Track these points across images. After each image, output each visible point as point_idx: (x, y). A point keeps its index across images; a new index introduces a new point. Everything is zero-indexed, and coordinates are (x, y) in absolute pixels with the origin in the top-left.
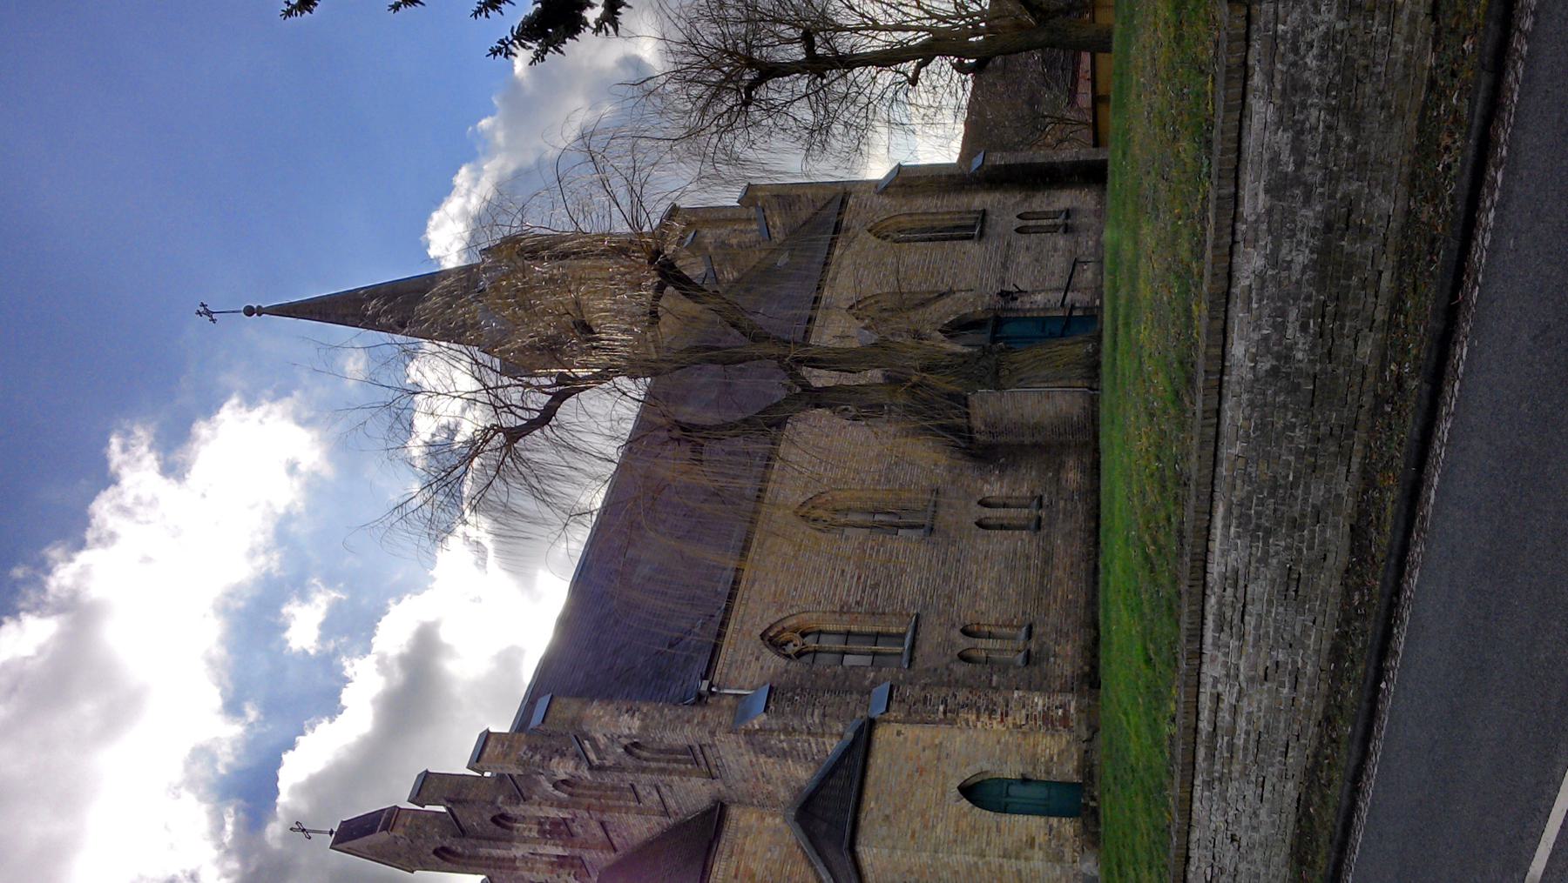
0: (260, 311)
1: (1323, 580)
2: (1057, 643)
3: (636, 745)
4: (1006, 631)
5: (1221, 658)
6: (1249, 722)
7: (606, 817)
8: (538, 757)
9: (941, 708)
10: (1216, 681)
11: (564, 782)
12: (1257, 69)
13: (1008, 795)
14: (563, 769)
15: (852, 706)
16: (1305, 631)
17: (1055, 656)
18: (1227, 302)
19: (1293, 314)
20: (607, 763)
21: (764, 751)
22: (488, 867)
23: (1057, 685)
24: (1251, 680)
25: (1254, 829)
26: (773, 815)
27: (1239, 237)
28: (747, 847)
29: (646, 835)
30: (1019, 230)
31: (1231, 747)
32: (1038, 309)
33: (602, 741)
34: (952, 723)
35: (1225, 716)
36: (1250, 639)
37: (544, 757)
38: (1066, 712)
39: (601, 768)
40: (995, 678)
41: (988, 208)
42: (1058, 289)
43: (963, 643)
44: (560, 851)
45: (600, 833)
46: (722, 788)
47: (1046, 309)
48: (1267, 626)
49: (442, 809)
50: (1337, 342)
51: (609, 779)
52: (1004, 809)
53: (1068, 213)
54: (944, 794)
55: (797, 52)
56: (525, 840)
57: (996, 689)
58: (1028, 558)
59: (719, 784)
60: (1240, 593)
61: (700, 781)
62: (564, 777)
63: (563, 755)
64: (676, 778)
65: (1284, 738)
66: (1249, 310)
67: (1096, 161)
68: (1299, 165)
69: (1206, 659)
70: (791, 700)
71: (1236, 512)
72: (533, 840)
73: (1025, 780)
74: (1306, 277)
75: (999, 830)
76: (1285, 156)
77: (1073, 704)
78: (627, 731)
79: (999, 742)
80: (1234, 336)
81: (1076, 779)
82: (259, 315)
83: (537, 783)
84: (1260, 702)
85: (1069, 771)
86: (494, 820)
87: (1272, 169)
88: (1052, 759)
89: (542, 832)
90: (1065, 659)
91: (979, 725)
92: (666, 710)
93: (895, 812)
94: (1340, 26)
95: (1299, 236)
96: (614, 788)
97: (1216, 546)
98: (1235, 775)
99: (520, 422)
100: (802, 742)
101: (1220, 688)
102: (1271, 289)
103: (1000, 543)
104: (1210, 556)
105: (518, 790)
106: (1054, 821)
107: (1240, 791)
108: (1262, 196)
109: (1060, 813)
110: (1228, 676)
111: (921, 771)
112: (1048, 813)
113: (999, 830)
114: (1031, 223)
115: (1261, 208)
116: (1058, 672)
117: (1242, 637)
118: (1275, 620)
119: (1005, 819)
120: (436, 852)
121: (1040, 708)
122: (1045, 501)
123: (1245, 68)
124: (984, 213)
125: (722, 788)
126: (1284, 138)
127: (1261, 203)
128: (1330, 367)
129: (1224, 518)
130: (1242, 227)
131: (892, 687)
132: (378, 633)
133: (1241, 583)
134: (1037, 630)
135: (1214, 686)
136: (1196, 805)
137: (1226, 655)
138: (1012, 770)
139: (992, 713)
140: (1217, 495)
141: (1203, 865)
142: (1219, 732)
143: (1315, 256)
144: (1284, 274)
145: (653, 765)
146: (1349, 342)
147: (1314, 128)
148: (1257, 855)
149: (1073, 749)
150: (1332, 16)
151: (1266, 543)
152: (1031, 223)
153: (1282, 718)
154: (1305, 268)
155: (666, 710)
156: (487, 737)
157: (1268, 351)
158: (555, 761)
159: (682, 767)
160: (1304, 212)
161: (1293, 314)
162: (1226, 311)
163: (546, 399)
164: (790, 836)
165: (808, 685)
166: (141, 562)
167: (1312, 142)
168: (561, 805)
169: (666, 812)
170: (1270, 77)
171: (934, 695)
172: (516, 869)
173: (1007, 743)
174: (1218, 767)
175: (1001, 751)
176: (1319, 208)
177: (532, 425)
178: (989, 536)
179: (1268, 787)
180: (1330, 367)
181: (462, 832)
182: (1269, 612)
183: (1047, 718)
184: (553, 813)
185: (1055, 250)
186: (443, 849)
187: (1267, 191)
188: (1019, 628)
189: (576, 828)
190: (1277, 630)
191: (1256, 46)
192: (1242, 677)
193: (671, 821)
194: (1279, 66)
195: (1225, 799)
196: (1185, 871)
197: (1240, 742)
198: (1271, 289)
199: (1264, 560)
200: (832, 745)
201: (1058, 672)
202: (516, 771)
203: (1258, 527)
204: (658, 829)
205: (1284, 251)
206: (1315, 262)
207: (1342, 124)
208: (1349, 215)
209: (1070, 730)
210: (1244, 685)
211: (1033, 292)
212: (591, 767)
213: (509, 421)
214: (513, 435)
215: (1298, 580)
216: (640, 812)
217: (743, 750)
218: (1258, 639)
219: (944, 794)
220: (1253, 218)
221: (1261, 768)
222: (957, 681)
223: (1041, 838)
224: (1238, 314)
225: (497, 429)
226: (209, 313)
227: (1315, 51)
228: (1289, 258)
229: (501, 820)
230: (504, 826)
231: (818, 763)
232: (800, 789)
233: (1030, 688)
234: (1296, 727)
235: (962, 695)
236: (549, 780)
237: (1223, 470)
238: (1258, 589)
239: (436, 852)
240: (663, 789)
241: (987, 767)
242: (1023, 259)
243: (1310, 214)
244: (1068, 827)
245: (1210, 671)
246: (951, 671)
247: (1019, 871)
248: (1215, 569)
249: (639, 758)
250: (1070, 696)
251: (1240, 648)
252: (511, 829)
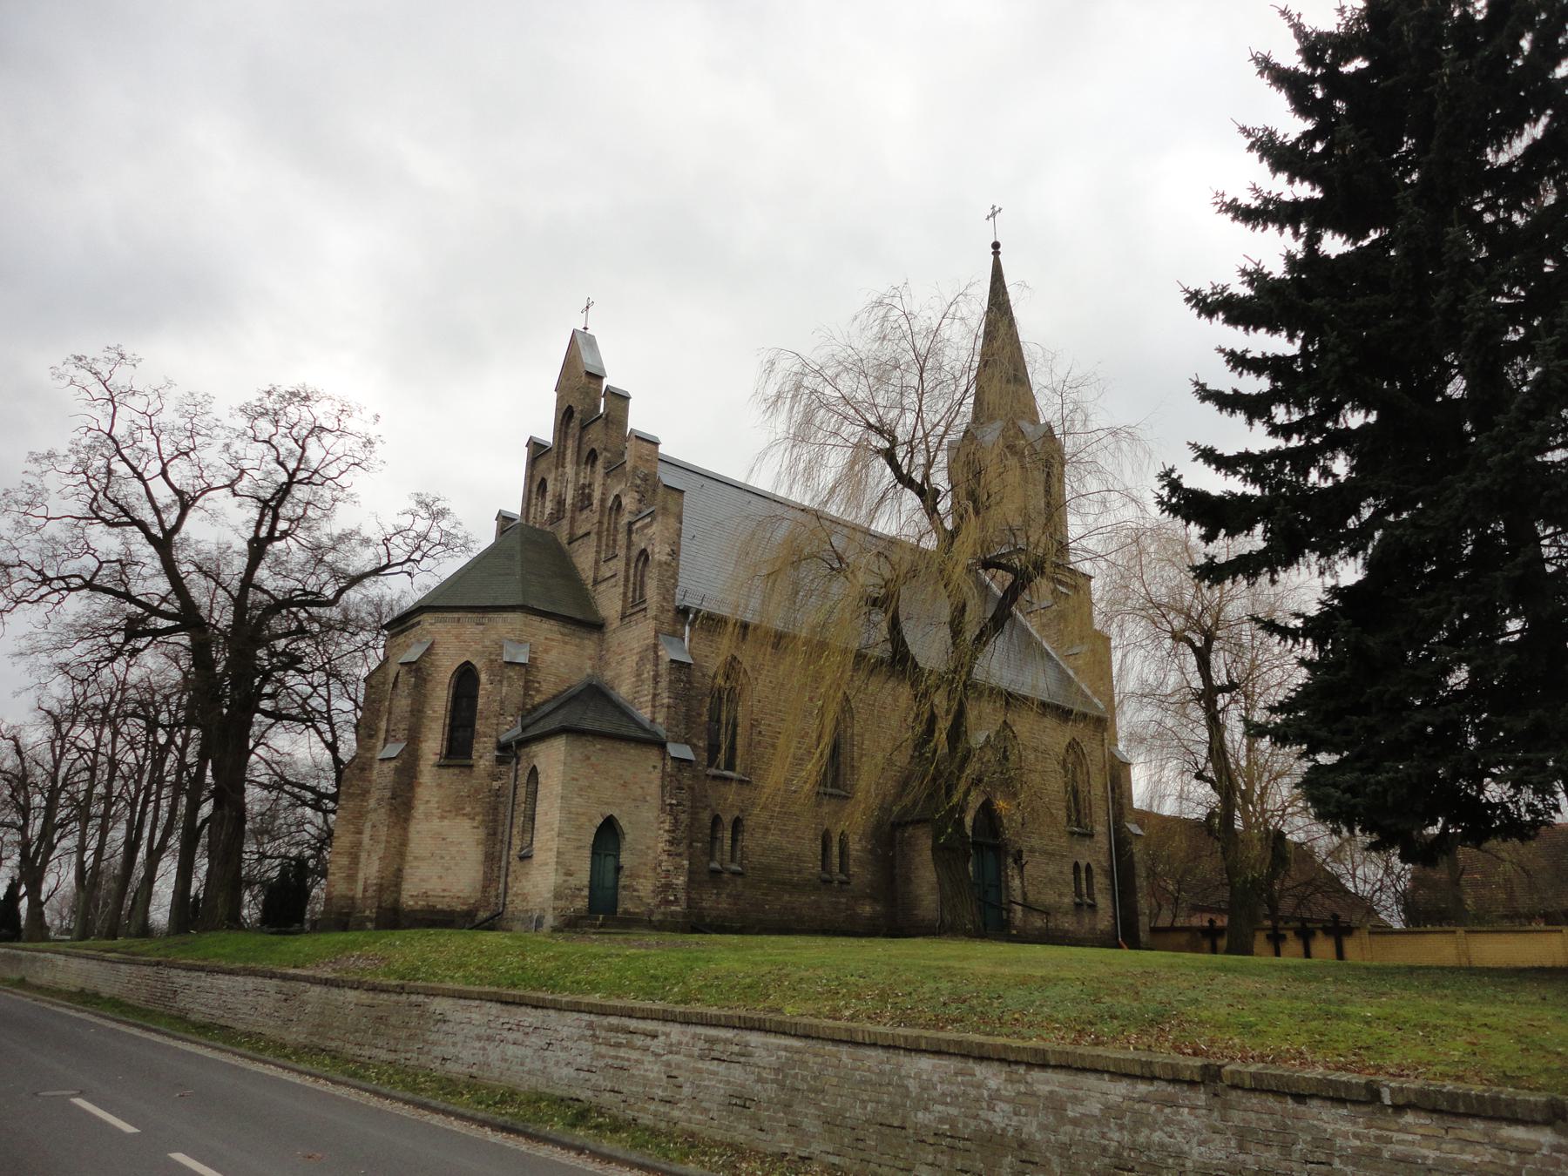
0: (996, 253)
1: (743, 1127)
3: (647, 559)
4: (739, 854)
5: (685, 1040)
6: (636, 1061)
7: (593, 536)
8: (638, 482)
9: (674, 802)
10: (667, 1035)
11: (620, 502)
12: (1151, 1088)
13: (606, 856)
14: (628, 502)
15: (675, 729)
16: (705, 1111)
18: (963, 1056)
19: (953, 1111)
20: (634, 535)
21: (641, 659)
22: (559, 447)
23: (694, 895)
24: (668, 1064)
25: (557, 1063)
26: (593, 667)
27: (1014, 1067)
28: (568, 647)
29: (579, 566)
30: (1076, 866)
31: (618, 1045)
32: (1007, 882)
33: (650, 531)
34: (663, 810)
35: (639, 1041)
36: (700, 1065)
37: (638, 487)
39: (630, 532)
41: (1096, 838)
42: (1024, 894)
43: (727, 819)
44: (569, 501)
45: (581, 532)
46: (614, 626)
47: (1008, 888)
48: (709, 1079)
49: (602, 411)
50: (931, 1148)
51: (622, 538)
52: (594, 853)
53: (1093, 907)
54: (607, 803)
55: (1220, 678)
56: (577, 474)
57: (690, 846)
58: (799, 872)
59: (616, 623)
60: (734, 1058)
61: (619, 608)
62: (623, 503)
63: (640, 501)
64: (621, 590)
65: (625, 1091)
66: (956, 1074)
67: (1138, 930)
68: (1075, 1122)
69: (684, 1028)
70: (681, 680)
71: (796, 1057)
72: (577, 480)
73: (618, 869)
74: (982, 1124)
75: (578, 848)
76: (1080, 1109)
77: (678, 909)
78: (657, 550)
79: (648, 848)
80: (936, 1061)
81: (620, 910)
83: (619, 482)
84: (652, 1071)
85: (626, 904)
86: (593, 451)
87: (1069, 1097)
88: (635, 890)
89: (584, 487)
90: (715, 902)
91: (661, 832)
93: (592, 765)
94: (1189, 1164)
95: (1016, 1118)
96: (615, 541)
97: (773, 1040)
98: (598, 1048)
99: (899, 460)
100: (647, 688)
101: (662, 1038)
102: (973, 1092)
103: (812, 848)
104: (763, 1034)
105: (614, 469)
106: (586, 892)
107: (583, 1052)
108: (1048, 1088)
109: (591, 897)
110: (671, 1045)
111: (625, 785)
112: (591, 888)
113: (578, 848)
114: (1083, 875)
115: (1037, 1087)
117: (701, 1058)
118: (714, 1086)
119: (587, 853)
120: (570, 407)
121: (675, 881)
122: (845, 887)
123: (1152, 1078)
124: (1091, 836)
125: (614, 626)
126: (1095, 1108)
127: (1041, 1087)
128: (911, 1141)
129: (792, 1047)
130: (1022, 1069)
131: (690, 761)
132: (1274, 88)
133: (742, 1059)
134: (739, 881)
135: (664, 1034)
136: (576, 1015)
137: (687, 1044)
138: (626, 859)
139: (671, 842)
140: (811, 1042)
141: (530, 1020)
142: (629, 1036)
143: (999, 1132)
144: (984, 1105)
145: (632, 571)
146: (930, 1158)
147: (1103, 1136)
148: (538, 1065)
150: (1196, 1157)
151: (773, 1081)
152: (1083, 875)
153: (640, 1089)
154: (989, 1122)
156: (656, 444)
157: (924, 1089)
158: (636, 496)
159: (630, 594)
160: (1035, 1124)
161: (953, 1111)
162: (954, 1054)
163: (919, 480)
164: (577, 680)
165: (693, 693)
167: (1092, 1133)
168: (603, 501)
169: (596, 582)
170: (1143, 1100)
171: (684, 795)
172: (557, 468)
173: (647, 855)
174: (603, 1034)
175: (641, 851)
176: (1038, 1137)
177: (896, 468)
178: (816, 839)
179: (588, 1075)
180: (911, 1141)
181: (584, 428)
182: (721, 1082)
183: (668, 887)
184: (597, 495)
185: (1060, 895)
186: (572, 412)
187: (1051, 1092)
188: (741, 865)
189: (586, 513)
190: (707, 1087)
191: (1170, 1089)
192: (670, 1056)
193: (589, 587)
194: (1153, 1108)
195: (579, 1039)
196: (527, 1005)
197: (622, 1053)
198: (973, 1092)
199: (760, 1080)
200: (645, 714)
201: (704, 896)
202: (628, 466)
203: (785, 1076)
204: (584, 576)
205: (1002, 1105)
206: (994, 1132)
207: (1107, 1161)
208: (1032, 1163)
209: (658, 906)
210: (664, 1058)
211: (1022, 878)
212: (630, 524)
213: (900, 453)
214: (890, 456)
215: (744, 1107)
216: (597, 562)
217: (642, 642)
218: (700, 1071)
219: (607, 803)
220: (1030, 1080)
221: (602, 1069)
222: (697, 813)
223: (573, 881)
224: (951, 1065)
225: (893, 441)
226: (994, 215)
227: (1167, 1140)
228: (997, 1109)
229: (592, 457)
230: (588, 458)
231: (632, 702)
232: (612, 688)
233: (692, 873)
234: (632, 1101)
235: (683, 817)
236: (621, 491)
237: (829, 1047)
238: (737, 1073)
239: (570, 407)
240: (613, 580)
241: (628, 838)
242: (1052, 869)
243: (1033, 1129)
244: (581, 904)
245: (676, 1032)
246: (705, 808)
247: (547, 864)
248: (754, 1038)
249: (638, 560)
250: (685, 906)
251: (691, 1056)
252: (586, 463)
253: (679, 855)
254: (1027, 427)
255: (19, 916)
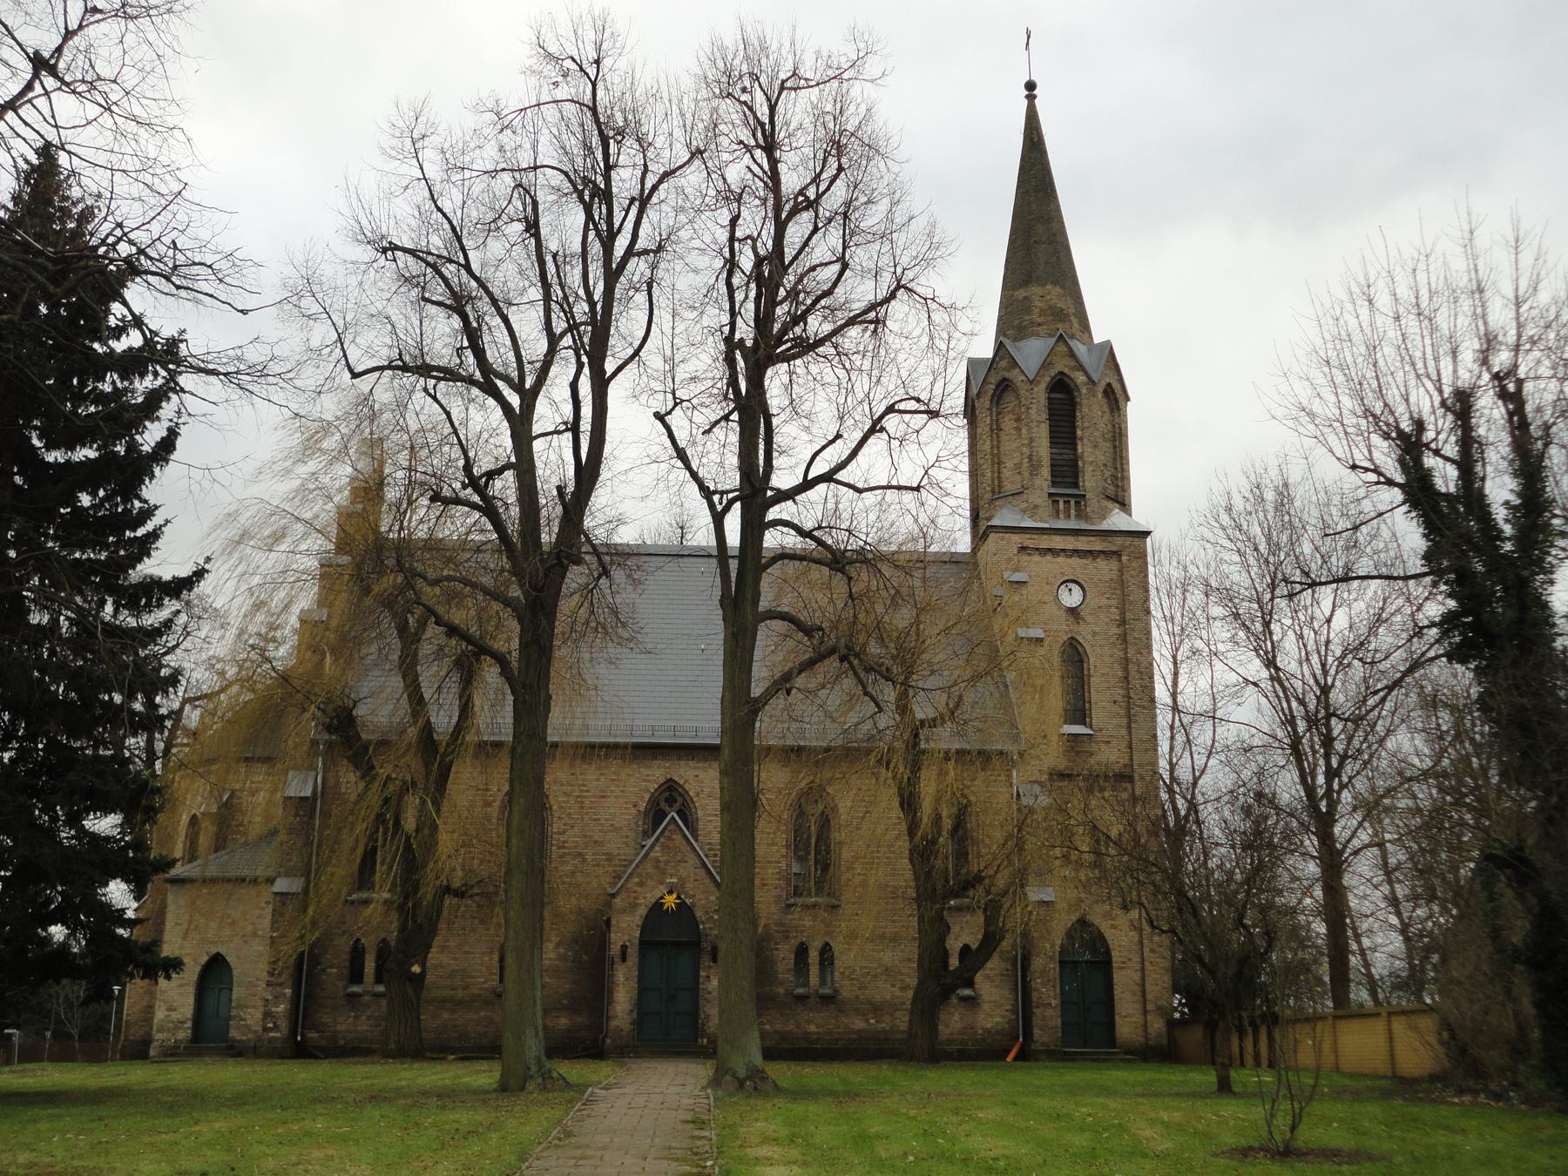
0: (1031, 98)
2: (369, 1018)
17: (355, 1017)
38: (271, 1030)
40: (335, 970)
54: (213, 943)
77: (278, 1035)
79: (258, 979)
82: (1027, 97)
92: (1472, 865)
106: (189, 1024)
116: (340, 1020)
121: (274, 1009)
149: (250, 1036)
155: (1472, 865)
166: (1148, 533)
223: (175, 1016)
244: (184, 1034)
253: (281, 984)
254: (1080, 349)
255: (758, 466)
